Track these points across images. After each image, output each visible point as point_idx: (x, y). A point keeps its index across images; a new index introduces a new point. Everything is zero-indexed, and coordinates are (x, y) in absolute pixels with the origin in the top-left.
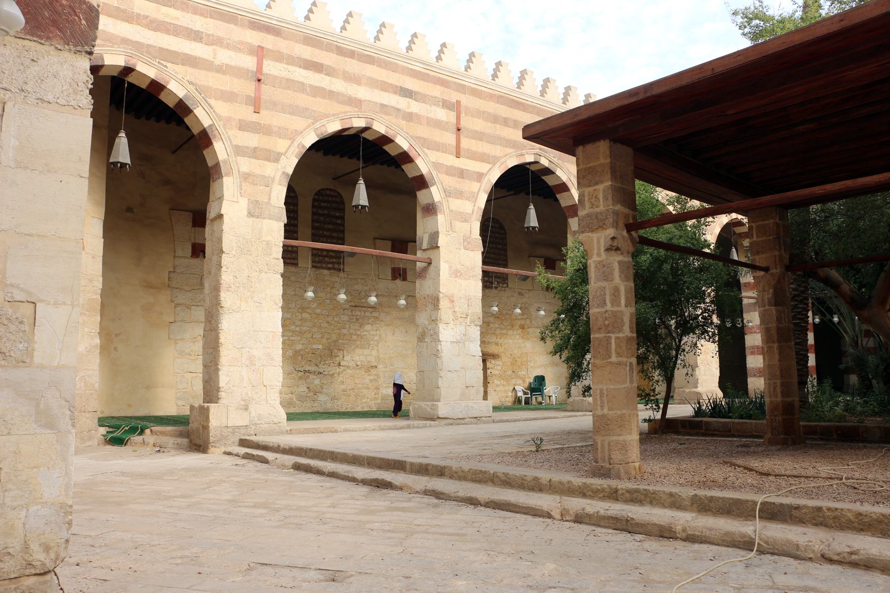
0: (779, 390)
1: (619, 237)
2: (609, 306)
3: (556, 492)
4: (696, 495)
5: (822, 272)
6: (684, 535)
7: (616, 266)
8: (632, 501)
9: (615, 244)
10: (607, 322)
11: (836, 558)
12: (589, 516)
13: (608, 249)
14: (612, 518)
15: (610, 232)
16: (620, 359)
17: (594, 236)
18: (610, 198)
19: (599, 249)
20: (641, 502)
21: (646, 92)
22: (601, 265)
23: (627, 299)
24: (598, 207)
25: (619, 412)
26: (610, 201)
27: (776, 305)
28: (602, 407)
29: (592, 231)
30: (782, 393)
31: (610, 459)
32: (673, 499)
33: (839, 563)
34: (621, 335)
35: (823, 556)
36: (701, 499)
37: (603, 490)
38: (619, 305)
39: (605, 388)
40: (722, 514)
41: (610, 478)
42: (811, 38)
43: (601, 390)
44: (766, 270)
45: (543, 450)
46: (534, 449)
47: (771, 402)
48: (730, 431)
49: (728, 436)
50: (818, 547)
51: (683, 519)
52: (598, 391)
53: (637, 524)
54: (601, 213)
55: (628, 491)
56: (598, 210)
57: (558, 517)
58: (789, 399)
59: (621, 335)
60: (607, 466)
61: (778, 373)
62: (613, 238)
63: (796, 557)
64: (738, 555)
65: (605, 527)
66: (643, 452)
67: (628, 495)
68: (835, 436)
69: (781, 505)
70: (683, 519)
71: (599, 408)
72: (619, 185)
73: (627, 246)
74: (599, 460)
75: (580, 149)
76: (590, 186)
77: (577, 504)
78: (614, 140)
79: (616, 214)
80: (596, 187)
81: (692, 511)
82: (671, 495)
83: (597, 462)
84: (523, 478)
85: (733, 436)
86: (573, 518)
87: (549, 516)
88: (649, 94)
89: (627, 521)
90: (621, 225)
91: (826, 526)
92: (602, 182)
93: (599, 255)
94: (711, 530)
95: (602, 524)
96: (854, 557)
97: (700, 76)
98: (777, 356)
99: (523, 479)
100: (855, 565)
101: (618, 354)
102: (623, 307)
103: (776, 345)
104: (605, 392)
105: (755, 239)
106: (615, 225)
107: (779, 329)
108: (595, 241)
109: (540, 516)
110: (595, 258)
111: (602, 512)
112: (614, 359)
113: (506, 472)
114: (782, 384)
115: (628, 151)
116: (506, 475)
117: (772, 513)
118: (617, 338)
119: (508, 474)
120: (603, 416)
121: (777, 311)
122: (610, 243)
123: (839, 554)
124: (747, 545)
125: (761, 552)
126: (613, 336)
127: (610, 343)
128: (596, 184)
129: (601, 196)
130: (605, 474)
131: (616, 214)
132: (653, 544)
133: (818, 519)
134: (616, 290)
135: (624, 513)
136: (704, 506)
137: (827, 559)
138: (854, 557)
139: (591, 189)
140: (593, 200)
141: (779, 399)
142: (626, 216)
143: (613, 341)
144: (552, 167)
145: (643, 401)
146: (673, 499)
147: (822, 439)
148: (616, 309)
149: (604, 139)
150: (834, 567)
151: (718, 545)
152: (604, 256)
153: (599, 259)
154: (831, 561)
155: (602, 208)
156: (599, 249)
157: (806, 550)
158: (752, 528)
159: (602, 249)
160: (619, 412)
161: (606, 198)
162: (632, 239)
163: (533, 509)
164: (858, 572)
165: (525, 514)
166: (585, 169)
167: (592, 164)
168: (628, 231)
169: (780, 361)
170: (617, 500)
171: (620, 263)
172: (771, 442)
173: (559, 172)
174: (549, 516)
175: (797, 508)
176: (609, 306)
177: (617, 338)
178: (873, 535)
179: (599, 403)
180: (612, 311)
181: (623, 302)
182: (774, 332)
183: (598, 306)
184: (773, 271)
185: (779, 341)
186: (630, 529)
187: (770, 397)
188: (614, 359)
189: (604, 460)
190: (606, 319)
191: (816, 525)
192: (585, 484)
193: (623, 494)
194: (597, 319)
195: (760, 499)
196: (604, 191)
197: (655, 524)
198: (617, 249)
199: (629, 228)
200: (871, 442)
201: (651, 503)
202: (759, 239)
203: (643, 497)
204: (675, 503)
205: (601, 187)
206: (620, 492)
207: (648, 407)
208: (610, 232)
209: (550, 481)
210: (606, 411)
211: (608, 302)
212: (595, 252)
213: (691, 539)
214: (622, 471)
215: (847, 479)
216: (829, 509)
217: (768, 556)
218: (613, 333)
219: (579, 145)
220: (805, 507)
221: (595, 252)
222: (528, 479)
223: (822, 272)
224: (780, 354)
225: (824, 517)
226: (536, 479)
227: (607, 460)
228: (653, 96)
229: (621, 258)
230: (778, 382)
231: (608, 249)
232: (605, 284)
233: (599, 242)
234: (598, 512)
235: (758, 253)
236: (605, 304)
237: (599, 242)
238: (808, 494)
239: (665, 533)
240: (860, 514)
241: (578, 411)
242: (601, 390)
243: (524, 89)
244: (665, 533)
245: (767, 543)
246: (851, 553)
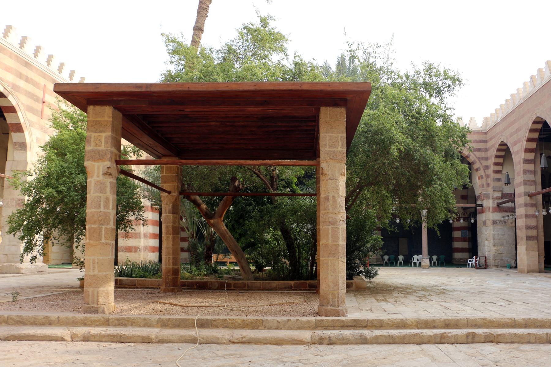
0: (171, 262)
1: (112, 167)
2: (102, 209)
3: (63, 324)
4: (160, 318)
5: (193, 197)
6: (157, 340)
7: (108, 184)
8: (119, 325)
9: (109, 171)
10: (100, 218)
11: (236, 341)
12: (93, 336)
13: (105, 174)
14: (110, 335)
15: (108, 164)
16: (107, 241)
17: (96, 164)
18: (109, 143)
19: (98, 173)
20: (125, 325)
21: (147, 88)
22: (98, 183)
23: (113, 206)
24: (100, 146)
25: (104, 273)
26: (109, 145)
27: (173, 214)
28: (94, 270)
29: (95, 161)
30: (173, 263)
31: (98, 301)
32: (146, 322)
33: (237, 343)
34: (108, 227)
35: (230, 341)
36: (163, 320)
37: (99, 320)
38: (108, 208)
39: (96, 258)
40: (175, 327)
41: (98, 313)
42: (240, 89)
43: (94, 260)
44: (169, 193)
45: (18, 300)
46: (11, 300)
47: (166, 268)
48: (135, 285)
49: (134, 288)
50: (228, 338)
51: (154, 332)
52: (91, 260)
53: (128, 337)
54: (102, 151)
55: (117, 320)
56: (100, 148)
57: (70, 339)
58: (176, 267)
59: (108, 227)
60: (96, 306)
61: (171, 252)
62: (109, 168)
63: (218, 343)
64: (191, 346)
65: (105, 342)
66: (117, 297)
67: (116, 322)
68: (195, 287)
69: (207, 319)
70: (154, 332)
71: (91, 270)
72: (114, 136)
73: (115, 172)
74: (90, 303)
75: (90, 108)
76: (96, 132)
77: (81, 330)
78: (115, 108)
79: (112, 152)
80: (100, 134)
81: (157, 327)
82: (145, 319)
83: (88, 304)
84: (35, 318)
85: (137, 288)
86: (81, 339)
87: (63, 339)
88: (148, 90)
89: (121, 336)
90: (113, 160)
91: (228, 327)
92: (104, 132)
93: (98, 176)
94: (172, 335)
95: (103, 340)
96: (244, 339)
97: (181, 89)
98: (171, 243)
99: (35, 319)
100: (244, 343)
101: (106, 238)
102: (110, 211)
103: (171, 236)
104: (97, 261)
105: (164, 174)
106: (110, 160)
107: (174, 227)
108: (96, 167)
109: (55, 341)
110: (95, 178)
111: (103, 333)
112: (103, 241)
113: (20, 315)
114: (173, 258)
115: (120, 115)
116: (20, 317)
117: (203, 324)
118: (106, 228)
119: (21, 316)
120: (94, 275)
121: (173, 217)
122: (106, 170)
123: (237, 339)
124: (193, 341)
125: (200, 343)
126: (104, 227)
127: (102, 231)
128: (101, 132)
129: (103, 140)
130: (95, 311)
131: (112, 152)
132: (140, 346)
133: (225, 325)
134: (107, 199)
135: (118, 332)
136: (164, 324)
137: (232, 342)
138: (244, 339)
139: (96, 134)
140: (97, 142)
141: (171, 266)
142: (116, 155)
143: (103, 230)
144: (5, 93)
145: (78, 267)
146: (146, 322)
147: (188, 289)
148: (106, 211)
149: (109, 105)
150: (235, 345)
151: (177, 343)
152: (101, 177)
153: (98, 179)
154: (234, 343)
155: (103, 147)
156: (98, 173)
157: (222, 340)
158: (194, 332)
159: (101, 173)
160: (104, 273)
161: (106, 142)
162: (118, 169)
163: (49, 336)
164: (246, 346)
165: (42, 340)
166: (93, 121)
167: (98, 119)
168: (116, 165)
169: (173, 245)
170: (109, 325)
171: (111, 183)
172: (165, 291)
173: (10, 98)
174: (63, 339)
175: (215, 320)
176: (102, 209)
177: (106, 228)
178: (249, 329)
179: (92, 267)
180: (104, 212)
181: (111, 207)
182: (171, 229)
183: (95, 208)
184: (173, 194)
185: (173, 234)
186: (122, 341)
187: (166, 265)
188: (103, 241)
189: (93, 303)
190: (100, 216)
191: (223, 328)
192: (86, 317)
193: (113, 321)
194: (93, 216)
195: (196, 318)
196: (106, 138)
197: (139, 336)
198: (110, 174)
199: (118, 162)
200: (213, 289)
201: (132, 325)
202: (167, 175)
203: (126, 322)
204: (147, 324)
205: (104, 135)
206: (111, 320)
207: (82, 270)
208: (108, 164)
209: (58, 317)
210: (96, 273)
211: (102, 206)
212: (96, 174)
213: (161, 341)
214: (106, 309)
215: (227, 306)
216: (230, 320)
217: (204, 345)
218: (104, 225)
219: (91, 105)
220: (219, 319)
221: (96, 174)
222: (40, 318)
223: (193, 197)
224: (173, 241)
225: (227, 324)
226: (46, 317)
227: (96, 302)
228: (151, 92)
229: (111, 180)
230: (171, 257)
231: (105, 174)
232: (101, 195)
233: (98, 168)
234: (100, 333)
235: (165, 182)
236: (100, 207)
237: (98, 168)
238: (213, 314)
239: (146, 340)
240: (244, 320)
241: (6, 273)
242: (94, 260)
243: (9, 39)
244: (146, 340)
245: (203, 338)
246: (243, 338)
